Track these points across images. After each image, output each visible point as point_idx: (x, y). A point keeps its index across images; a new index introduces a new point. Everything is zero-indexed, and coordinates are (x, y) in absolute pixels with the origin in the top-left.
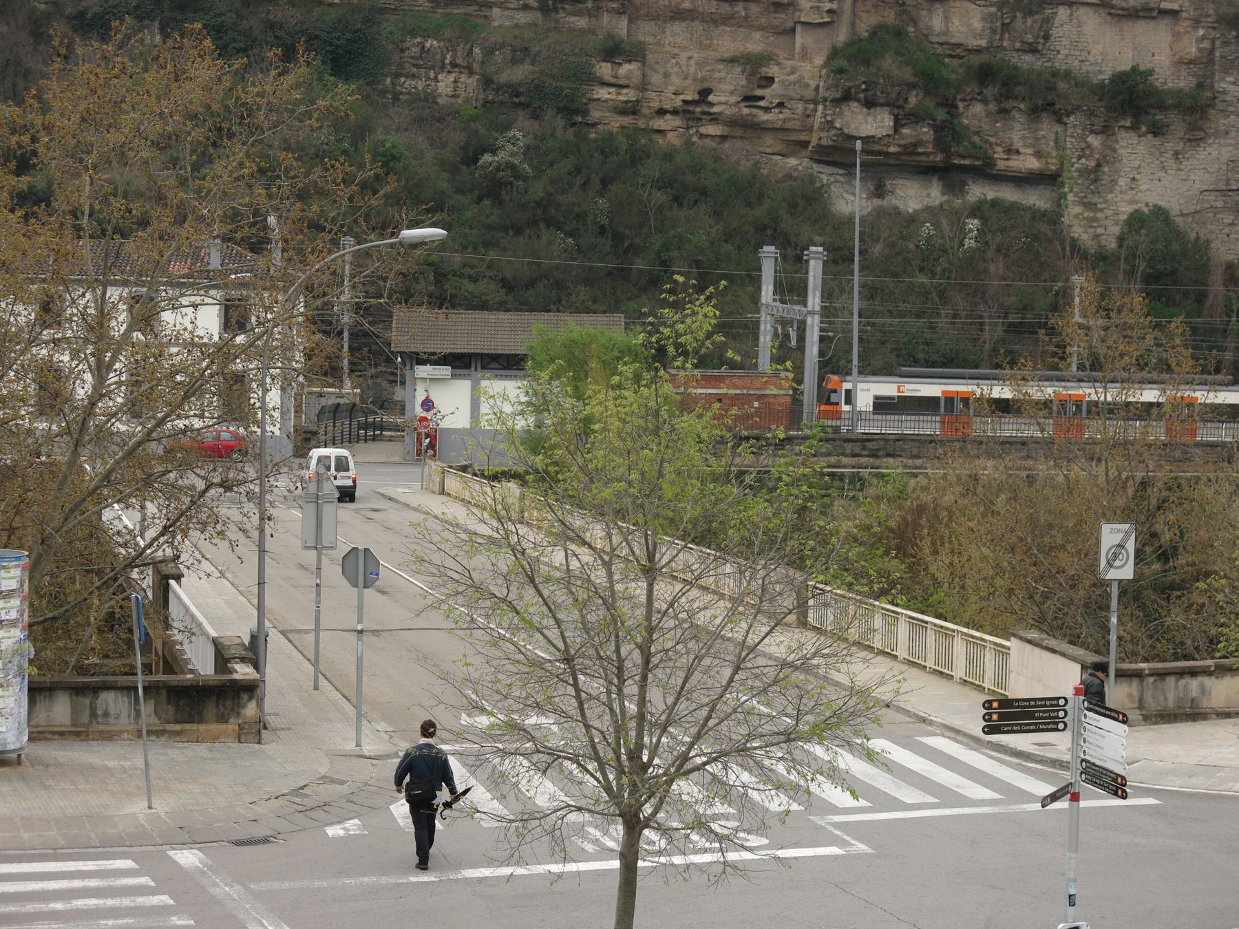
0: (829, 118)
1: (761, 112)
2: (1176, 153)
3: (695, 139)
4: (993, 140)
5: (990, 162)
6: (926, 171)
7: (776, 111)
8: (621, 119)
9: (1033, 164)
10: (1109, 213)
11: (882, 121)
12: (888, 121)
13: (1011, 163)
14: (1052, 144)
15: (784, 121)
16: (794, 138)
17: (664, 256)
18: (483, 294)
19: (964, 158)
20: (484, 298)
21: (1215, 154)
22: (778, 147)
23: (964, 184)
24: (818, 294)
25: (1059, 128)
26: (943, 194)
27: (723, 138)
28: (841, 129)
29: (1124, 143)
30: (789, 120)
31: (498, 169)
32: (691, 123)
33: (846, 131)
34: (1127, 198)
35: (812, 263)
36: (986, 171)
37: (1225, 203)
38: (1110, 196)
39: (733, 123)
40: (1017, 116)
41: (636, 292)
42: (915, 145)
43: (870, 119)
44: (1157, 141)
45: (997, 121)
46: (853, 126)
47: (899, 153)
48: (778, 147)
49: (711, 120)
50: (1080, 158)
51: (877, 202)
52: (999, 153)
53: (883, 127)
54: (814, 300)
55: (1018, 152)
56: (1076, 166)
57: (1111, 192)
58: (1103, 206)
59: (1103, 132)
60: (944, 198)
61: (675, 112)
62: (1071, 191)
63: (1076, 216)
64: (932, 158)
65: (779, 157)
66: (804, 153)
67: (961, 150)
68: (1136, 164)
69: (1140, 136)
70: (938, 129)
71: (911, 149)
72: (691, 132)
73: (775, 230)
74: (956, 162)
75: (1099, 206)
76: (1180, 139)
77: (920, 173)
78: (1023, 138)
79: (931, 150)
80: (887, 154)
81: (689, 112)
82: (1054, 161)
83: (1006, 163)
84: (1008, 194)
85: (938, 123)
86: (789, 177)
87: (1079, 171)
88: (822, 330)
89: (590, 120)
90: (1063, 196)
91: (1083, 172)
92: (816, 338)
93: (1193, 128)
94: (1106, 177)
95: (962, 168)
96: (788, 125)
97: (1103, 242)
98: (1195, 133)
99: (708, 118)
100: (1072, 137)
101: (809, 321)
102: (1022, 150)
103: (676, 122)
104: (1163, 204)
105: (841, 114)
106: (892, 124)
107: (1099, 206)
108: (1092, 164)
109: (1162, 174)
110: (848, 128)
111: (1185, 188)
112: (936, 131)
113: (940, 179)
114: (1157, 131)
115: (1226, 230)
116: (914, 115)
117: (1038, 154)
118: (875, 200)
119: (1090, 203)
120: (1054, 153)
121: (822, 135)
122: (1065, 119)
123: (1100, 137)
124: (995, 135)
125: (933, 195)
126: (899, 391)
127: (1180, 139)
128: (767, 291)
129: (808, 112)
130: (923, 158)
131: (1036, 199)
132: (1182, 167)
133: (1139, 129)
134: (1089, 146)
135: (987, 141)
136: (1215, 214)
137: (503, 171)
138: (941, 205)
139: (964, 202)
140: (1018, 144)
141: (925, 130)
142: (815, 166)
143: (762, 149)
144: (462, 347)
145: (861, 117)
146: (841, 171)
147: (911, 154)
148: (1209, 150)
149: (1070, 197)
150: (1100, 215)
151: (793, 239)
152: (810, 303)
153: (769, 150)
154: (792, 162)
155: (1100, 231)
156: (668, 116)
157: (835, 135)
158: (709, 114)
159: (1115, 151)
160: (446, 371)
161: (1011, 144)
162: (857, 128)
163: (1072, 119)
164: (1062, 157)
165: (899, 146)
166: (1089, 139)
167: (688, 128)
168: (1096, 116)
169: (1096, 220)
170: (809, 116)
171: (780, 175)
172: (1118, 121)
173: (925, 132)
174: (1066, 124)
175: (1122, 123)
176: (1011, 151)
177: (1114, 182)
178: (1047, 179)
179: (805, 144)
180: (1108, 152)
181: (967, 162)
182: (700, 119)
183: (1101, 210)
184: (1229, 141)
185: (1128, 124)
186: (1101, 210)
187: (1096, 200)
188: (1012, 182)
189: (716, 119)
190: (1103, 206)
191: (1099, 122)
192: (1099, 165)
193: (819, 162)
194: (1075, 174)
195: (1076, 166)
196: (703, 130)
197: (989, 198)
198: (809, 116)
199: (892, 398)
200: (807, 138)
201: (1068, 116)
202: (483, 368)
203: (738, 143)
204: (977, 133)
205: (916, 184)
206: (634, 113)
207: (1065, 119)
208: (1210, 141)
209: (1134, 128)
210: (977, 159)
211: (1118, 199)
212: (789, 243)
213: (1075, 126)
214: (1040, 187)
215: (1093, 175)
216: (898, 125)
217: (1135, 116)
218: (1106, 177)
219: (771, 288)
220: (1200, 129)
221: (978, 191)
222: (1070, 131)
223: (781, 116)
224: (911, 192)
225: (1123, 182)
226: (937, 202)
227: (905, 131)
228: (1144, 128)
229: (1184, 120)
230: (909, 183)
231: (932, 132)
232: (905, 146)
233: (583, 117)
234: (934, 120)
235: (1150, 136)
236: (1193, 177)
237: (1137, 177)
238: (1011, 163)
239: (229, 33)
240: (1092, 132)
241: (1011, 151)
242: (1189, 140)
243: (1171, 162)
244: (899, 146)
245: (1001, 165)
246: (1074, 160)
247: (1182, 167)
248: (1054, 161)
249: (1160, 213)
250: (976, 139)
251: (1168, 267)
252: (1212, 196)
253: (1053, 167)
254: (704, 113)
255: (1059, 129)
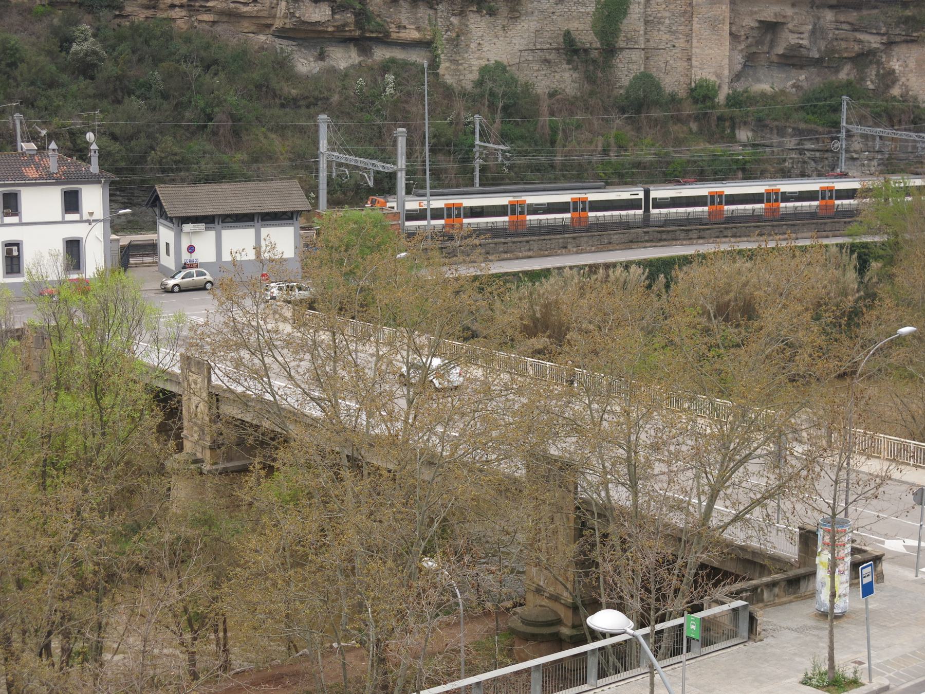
0: (292, 11)
1: (241, 6)
2: (504, 27)
3: (196, 24)
4: (389, 20)
5: (387, 34)
6: (346, 41)
7: (252, 5)
8: (146, 12)
9: (415, 35)
10: (466, 66)
11: (325, 12)
12: (328, 12)
13: (401, 35)
14: (427, 22)
15: (258, 11)
16: (263, 22)
17: (208, 110)
18: (107, 147)
19: (372, 32)
20: (108, 149)
21: (526, 26)
22: (253, 28)
23: (371, 49)
24: (404, 157)
25: (431, 12)
26: (359, 56)
27: (214, 23)
28: (299, 18)
29: (472, 21)
30: (261, 10)
31: (86, 55)
32: (192, 13)
33: (303, 19)
34: (476, 56)
35: (400, 138)
36: (385, 41)
37: (534, 57)
38: (466, 55)
39: (221, 13)
40: (403, 4)
41: (188, 135)
42: (344, 26)
43: (317, 10)
44: (492, 19)
45: (391, 8)
46: (307, 15)
47: (334, 31)
48: (253, 28)
49: (206, 11)
50: (447, 31)
51: (321, 63)
52: (393, 28)
53: (325, 15)
54: (402, 162)
55: (405, 27)
56: (445, 36)
57: (467, 52)
58: (462, 61)
59: (460, 15)
60: (361, 59)
61: (182, 6)
62: (443, 53)
63: (447, 68)
64: (353, 33)
65: (252, 35)
66: (267, 32)
67: (371, 28)
68: (480, 34)
69: (482, 16)
70: (357, 15)
71: (341, 28)
72: (193, 19)
73: (267, 87)
74: (368, 35)
75: (460, 62)
76: (506, 17)
77: (342, 42)
78: (408, 18)
79: (353, 28)
80: (327, 32)
81: (191, 5)
82: (429, 33)
83: (397, 34)
84: (399, 54)
85: (357, 11)
86: (262, 48)
87: (446, 39)
88: (407, 179)
89: (124, 13)
90: (437, 56)
91: (450, 40)
92: (404, 185)
93: (513, 10)
94: (463, 43)
95: (371, 39)
96: (260, 14)
97: (464, 85)
98: (514, 13)
99: (204, 9)
100: (441, 18)
101: (399, 174)
102: (408, 26)
103: (183, 13)
104: (498, 59)
105: (299, 7)
106: (330, 13)
107: (460, 62)
108: (454, 35)
109: (496, 40)
110: (304, 16)
111: (510, 49)
112: (356, 16)
113: (355, 46)
114: (492, 13)
115: (535, 74)
116: (342, 6)
117: (418, 29)
118: (319, 62)
119: (454, 60)
120: (429, 28)
121: (286, 21)
122: (436, 7)
123: (458, 18)
124: (390, 17)
125: (353, 57)
126: (420, 206)
127: (506, 17)
128: (323, 145)
129: (273, 5)
130: (348, 34)
131: (419, 58)
132: (507, 35)
133: (482, 12)
134: (451, 24)
135: (385, 21)
136: (528, 64)
137: (89, 56)
138: (360, 63)
139: (373, 61)
140: (405, 22)
141: (349, 15)
142: (276, 40)
143: (241, 30)
144: (210, 211)
145: (311, 9)
146: (294, 43)
147: (342, 31)
148: (523, 24)
149: (442, 57)
150: (460, 67)
151: (278, 92)
152: (399, 164)
153: (246, 30)
154: (262, 38)
155: (462, 77)
156: (177, 9)
157: (296, 22)
158: (205, 7)
159: (467, 26)
160: (201, 226)
161: (400, 23)
162: (309, 17)
163: (440, 6)
164: (434, 30)
165: (334, 26)
166: (451, 19)
167: (190, 17)
168: (456, 4)
169: (459, 70)
170: (273, 8)
171: (257, 47)
172: (468, 7)
173: (349, 17)
174: (436, 9)
175: (471, 8)
176: (401, 27)
177: (468, 46)
178: (425, 44)
179: (269, 26)
180: (463, 27)
181: (374, 35)
182: (198, 10)
183: (461, 64)
184: (533, 18)
185: (475, 9)
186: (461, 64)
187: (458, 58)
188: (399, 46)
189: (210, 10)
190: (462, 61)
191: (457, 8)
192: (458, 36)
193: (278, 37)
194: (444, 42)
195: (445, 36)
196: (200, 18)
197: (387, 57)
198: (273, 8)
199: (416, 210)
200: (272, 22)
201: (438, 4)
202: (222, 222)
203: (225, 26)
204: (379, 16)
205: (341, 50)
206: (154, 8)
207: (436, 7)
208: (523, 18)
209: (479, 11)
210: (380, 33)
211: (471, 57)
212: (276, 96)
213: (442, 11)
214: (417, 49)
215: (455, 42)
216: (334, 13)
217: (478, 4)
218: (463, 43)
219: (325, 141)
220: (517, 11)
221: (381, 54)
222: (439, 14)
223: (255, 8)
224: (339, 55)
225: (473, 46)
226: (357, 62)
227: (337, 17)
228: (485, 12)
229: (507, 6)
230: (337, 50)
231: (353, 17)
232: (337, 27)
233: (120, 11)
234: (354, 9)
235: (487, 16)
236: (514, 41)
237: (481, 42)
238: (401, 35)
239: (553, 177)
240: (453, 15)
241: (401, 27)
242: (511, 18)
243: (501, 33)
244: (334, 26)
245: (394, 36)
246: (443, 33)
247: (507, 35)
248: (429, 33)
249: (500, 67)
250: (378, 19)
251: (512, 101)
252: (526, 53)
253: (428, 37)
254: (201, 6)
255: (431, 12)
